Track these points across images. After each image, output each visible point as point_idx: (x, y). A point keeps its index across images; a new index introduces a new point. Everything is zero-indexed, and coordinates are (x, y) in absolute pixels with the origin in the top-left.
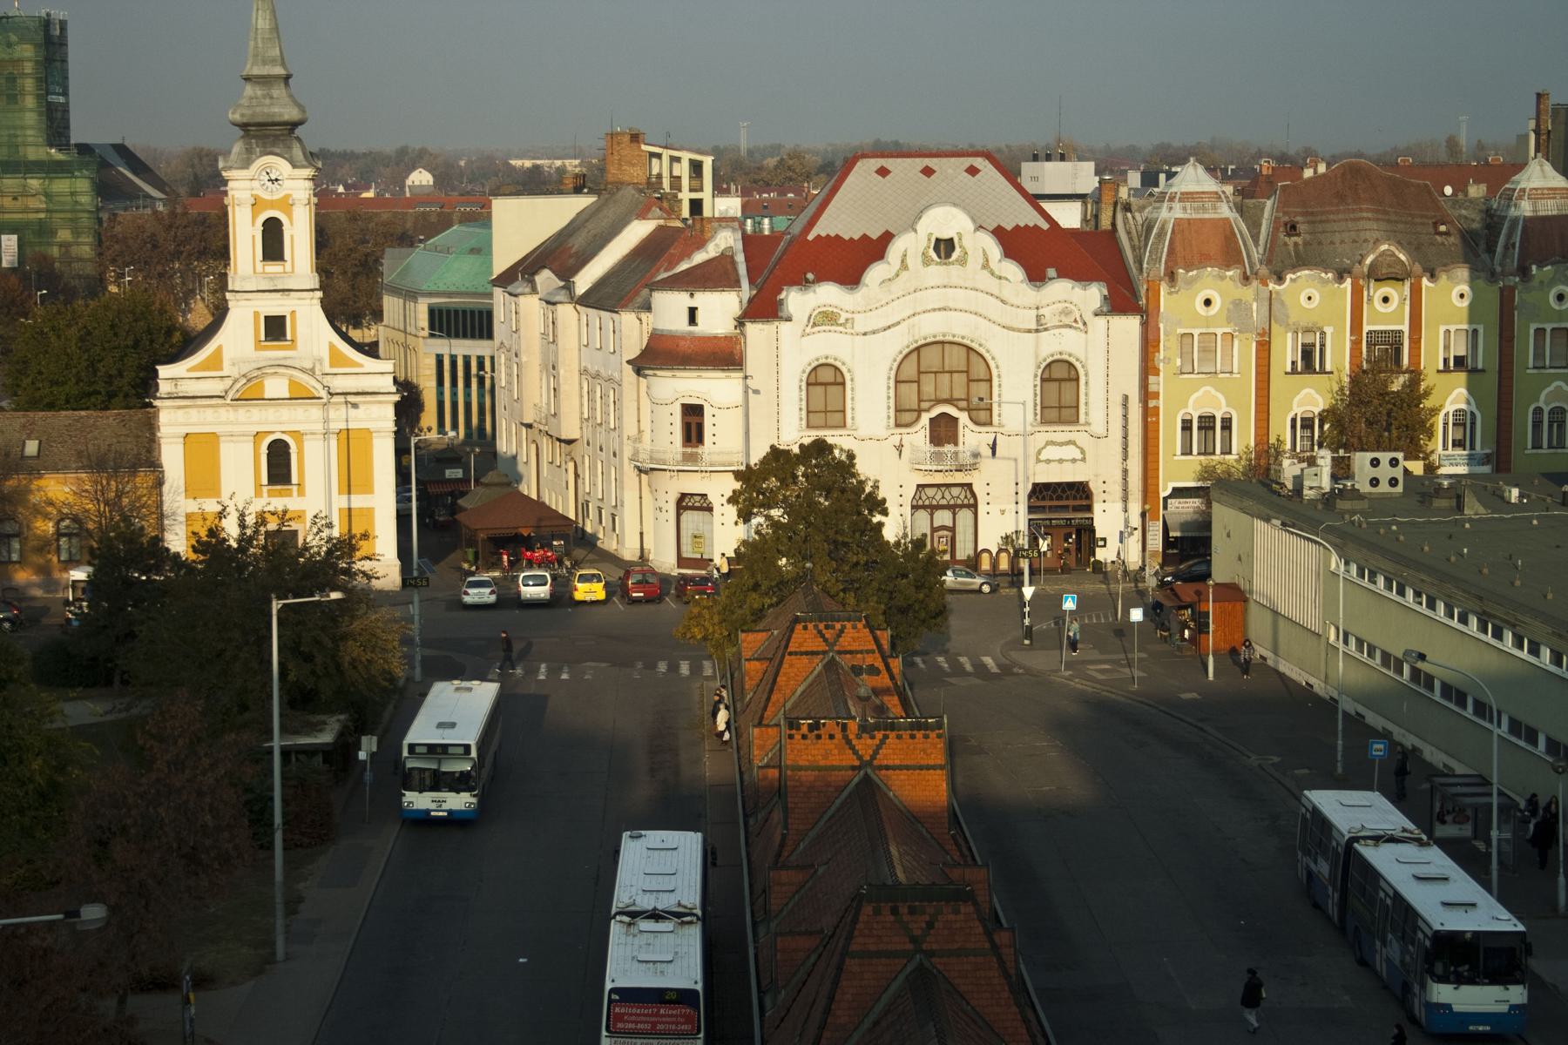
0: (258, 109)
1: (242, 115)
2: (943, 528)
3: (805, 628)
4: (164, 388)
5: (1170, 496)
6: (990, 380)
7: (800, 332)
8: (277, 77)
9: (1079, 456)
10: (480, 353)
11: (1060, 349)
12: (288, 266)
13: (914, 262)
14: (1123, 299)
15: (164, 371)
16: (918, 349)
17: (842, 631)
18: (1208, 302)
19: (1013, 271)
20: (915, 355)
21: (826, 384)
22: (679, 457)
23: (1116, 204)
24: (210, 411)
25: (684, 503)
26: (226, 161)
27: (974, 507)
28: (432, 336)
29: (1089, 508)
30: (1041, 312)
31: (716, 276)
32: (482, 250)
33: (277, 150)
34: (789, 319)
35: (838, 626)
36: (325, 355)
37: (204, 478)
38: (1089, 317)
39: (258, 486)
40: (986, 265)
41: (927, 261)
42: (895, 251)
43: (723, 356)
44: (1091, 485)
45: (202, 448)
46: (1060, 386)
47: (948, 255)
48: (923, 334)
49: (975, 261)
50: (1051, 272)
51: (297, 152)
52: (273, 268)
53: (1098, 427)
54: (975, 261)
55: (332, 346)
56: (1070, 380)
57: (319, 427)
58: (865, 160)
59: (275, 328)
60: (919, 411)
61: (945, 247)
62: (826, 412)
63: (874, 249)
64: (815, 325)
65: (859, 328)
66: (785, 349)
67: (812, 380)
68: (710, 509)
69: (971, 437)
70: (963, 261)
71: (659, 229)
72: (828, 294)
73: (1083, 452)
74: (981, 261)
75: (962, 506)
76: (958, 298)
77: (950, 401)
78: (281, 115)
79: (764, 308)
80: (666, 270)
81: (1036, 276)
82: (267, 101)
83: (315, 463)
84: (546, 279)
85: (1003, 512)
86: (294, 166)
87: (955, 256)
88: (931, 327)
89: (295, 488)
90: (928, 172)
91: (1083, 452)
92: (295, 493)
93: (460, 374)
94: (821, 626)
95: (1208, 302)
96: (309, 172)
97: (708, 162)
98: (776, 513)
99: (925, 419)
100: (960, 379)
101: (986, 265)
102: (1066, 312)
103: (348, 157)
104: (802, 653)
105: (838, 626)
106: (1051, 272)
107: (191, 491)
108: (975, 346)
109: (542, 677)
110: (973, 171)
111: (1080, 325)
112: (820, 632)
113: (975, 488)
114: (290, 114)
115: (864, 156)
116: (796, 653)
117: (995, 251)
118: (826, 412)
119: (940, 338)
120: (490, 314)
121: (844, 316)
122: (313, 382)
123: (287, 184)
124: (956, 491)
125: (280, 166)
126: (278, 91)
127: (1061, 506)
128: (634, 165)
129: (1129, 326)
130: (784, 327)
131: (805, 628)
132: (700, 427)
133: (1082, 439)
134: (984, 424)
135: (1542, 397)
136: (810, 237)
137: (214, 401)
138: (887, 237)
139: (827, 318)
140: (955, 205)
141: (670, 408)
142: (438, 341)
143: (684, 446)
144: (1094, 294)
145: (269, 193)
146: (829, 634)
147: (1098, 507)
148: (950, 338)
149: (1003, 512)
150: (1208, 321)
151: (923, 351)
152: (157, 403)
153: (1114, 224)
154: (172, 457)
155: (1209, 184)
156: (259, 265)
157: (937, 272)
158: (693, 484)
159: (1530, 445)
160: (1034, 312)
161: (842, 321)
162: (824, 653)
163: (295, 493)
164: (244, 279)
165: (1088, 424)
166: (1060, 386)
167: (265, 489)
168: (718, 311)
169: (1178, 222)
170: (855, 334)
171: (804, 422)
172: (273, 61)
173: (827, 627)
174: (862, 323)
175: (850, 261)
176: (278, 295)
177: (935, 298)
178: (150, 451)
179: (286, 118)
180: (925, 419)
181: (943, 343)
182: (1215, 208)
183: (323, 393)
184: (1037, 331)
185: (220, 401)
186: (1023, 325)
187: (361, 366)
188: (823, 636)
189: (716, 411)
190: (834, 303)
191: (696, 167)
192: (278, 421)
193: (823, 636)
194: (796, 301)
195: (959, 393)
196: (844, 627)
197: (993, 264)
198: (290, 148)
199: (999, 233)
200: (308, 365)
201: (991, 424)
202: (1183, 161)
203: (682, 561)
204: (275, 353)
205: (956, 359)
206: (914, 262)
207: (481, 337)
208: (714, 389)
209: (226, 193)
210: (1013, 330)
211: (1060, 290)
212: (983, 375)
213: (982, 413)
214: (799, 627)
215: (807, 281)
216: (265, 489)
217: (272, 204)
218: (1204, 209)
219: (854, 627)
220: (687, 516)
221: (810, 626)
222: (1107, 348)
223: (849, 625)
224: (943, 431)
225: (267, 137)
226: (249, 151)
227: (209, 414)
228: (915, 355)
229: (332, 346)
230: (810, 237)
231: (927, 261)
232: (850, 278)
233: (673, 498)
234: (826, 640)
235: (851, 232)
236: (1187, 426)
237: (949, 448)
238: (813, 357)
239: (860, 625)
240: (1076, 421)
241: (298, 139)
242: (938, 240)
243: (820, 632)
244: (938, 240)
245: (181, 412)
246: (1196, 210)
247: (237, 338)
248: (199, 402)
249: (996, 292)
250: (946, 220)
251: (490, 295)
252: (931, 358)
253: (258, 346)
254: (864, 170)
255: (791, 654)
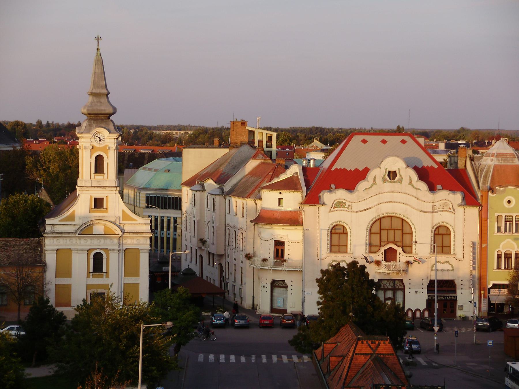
0: (95, 108)
1: (88, 110)
2: (389, 299)
3: (362, 343)
4: (48, 229)
5: (491, 288)
6: (412, 234)
7: (328, 210)
8: (103, 94)
9: (451, 268)
10: (168, 215)
11: (339, 220)
12: (106, 176)
13: (379, 181)
14: (470, 199)
15: (48, 221)
16: (380, 219)
17: (379, 345)
18: (509, 202)
19: (423, 186)
20: (378, 222)
21: (338, 235)
22: (272, 264)
23: (466, 157)
24: (68, 239)
25: (274, 284)
26: (80, 130)
27: (403, 290)
28: (147, 207)
29: (455, 292)
30: (435, 204)
31: (290, 185)
32: (180, 171)
33: (103, 126)
34: (324, 204)
35: (377, 342)
36: (121, 215)
37: (64, 270)
38: (455, 207)
39: (88, 273)
40: (410, 183)
41: (384, 181)
42: (370, 176)
43: (293, 220)
44: (456, 282)
45: (65, 255)
46: (441, 237)
47: (394, 178)
48: (382, 212)
49: (406, 181)
50: (439, 187)
51: (112, 127)
52: (99, 177)
53: (460, 256)
54: (406, 181)
55: (123, 212)
56: (447, 234)
57: (117, 248)
58: (357, 136)
59: (98, 203)
60: (380, 246)
61: (392, 175)
62: (339, 246)
63: (361, 175)
64: (334, 208)
65: (354, 209)
66: (321, 218)
67: (436, 232)
68: (286, 287)
69: (402, 257)
70: (400, 181)
71: (262, 163)
72: (341, 194)
73: (452, 267)
74: (409, 181)
75: (390, 289)
76: (397, 197)
77: (394, 242)
78: (105, 110)
79: (312, 199)
80: (267, 182)
81: (432, 188)
82: (99, 104)
83: (113, 263)
84: (210, 183)
85: (416, 292)
86: (110, 132)
87: (397, 178)
88: (386, 209)
89: (105, 274)
90: (384, 142)
91: (452, 267)
92: (105, 276)
93: (165, 225)
94: (370, 342)
95: (509, 202)
96: (115, 135)
97: (275, 135)
98: (374, 292)
99: (383, 250)
100: (398, 233)
101: (410, 183)
102: (445, 205)
103: (461, 133)
104: (361, 354)
105: (377, 342)
106: (439, 187)
107: (58, 274)
108: (405, 218)
109: (253, 361)
110: (403, 142)
111: (452, 210)
112: (369, 345)
113: (404, 281)
114: (110, 110)
115: (356, 134)
116: (358, 354)
117: (414, 176)
118: (339, 246)
119: (390, 215)
120: (181, 199)
121: (348, 204)
122: (115, 227)
123: (107, 140)
124: (281, 282)
125: (104, 133)
126: (104, 100)
127: (443, 290)
128: (242, 136)
129: (474, 212)
130: (322, 208)
131: (362, 343)
132: (283, 251)
133: (452, 261)
134: (409, 253)
135: (501, 246)
136: (333, 169)
137: (70, 235)
138: (366, 170)
139: (340, 204)
140: (398, 157)
141: (269, 242)
142: (151, 210)
143: (275, 259)
144: (458, 197)
145: (96, 145)
146: (373, 346)
147: (459, 292)
148: (394, 215)
149: (416, 292)
150: (509, 210)
151: (383, 220)
152: (45, 235)
153: (465, 166)
154: (50, 259)
155: (510, 150)
156: (93, 175)
157: (389, 186)
158: (279, 277)
159: (495, 267)
160: (431, 204)
161: (347, 206)
162: (372, 354)
163: (105, 276)
164: (86, 181)
165: (455, 254)
166: (441, 237)
167: (91, 274)
168: (292, 200)
169: (495, 166)
170: (354, 212)
171: (329, 250)
172: (102, 87)
173: (372, 343)
174: (356, 207)
175: (350, 180)
176: (101, 189)
177: (387, 197)
178: (40, 256)
179: (107, 112)
180: (383, 250)
181: (391, 217)
182: (512, 160)
183: (119, 232)
184: (433, 212)
185: (73, 235)
186: (424, 209)
187: (136, 220)
188: (370, 347)
189: (290, 244)
190: (344, 198)
191: (270, 138)
192: (98, 245)
193: (370, 347)
194: (327, 197)
195: (398, 239)
196: (379, 343)
197: (414, 183)
198: (108, 124)
199: (416, 169)
200: (113, 220)
201: (412, 253)
202: (498, 138)
203: (273, 310)
204: (98, 214)
205: (397, 224)
206: (379, 181)
207: (177, 209)
208: (290, 235)
209: (78, 143)
210: (424, 212)
211: (444, 196)
212: (408, 231)
213: (407, 249)
214: (360, 342)
215: (331, 188)
216: (91, 274)
217: (100, 149)
218: (508, 161)
219: (384, 343)
220: (277, 291)
221: (365, 342)
222: (462, 221)
223: (382, 342)
224: (390, 255)
225: (97, 119)
226: (90, 125)
227: (68, 241)
228: (378, 222)
229: (123, 212)
230: (333, 169)
231: (384, 181)
232: (350, 188)
233: (269, 282)
234: (372, 349)
235: (350, 167)
236: (499, 257)
237: (393, 263)
238: (338, 220)
239: (387, 342)
240: (449, 252)
241: (111, 120)
242: (389, 172)
243: (369, 345)
244: (389, 172)
245: (55, 240)
246: (504, 161)
247: (81, 207)
248: (64, 235)
249: (415, 195)
250: (395, 163)
251: (181, 191)
252: (386, 224)
253: (91, 211)
254: (357, 139)
255: (356, 354)
